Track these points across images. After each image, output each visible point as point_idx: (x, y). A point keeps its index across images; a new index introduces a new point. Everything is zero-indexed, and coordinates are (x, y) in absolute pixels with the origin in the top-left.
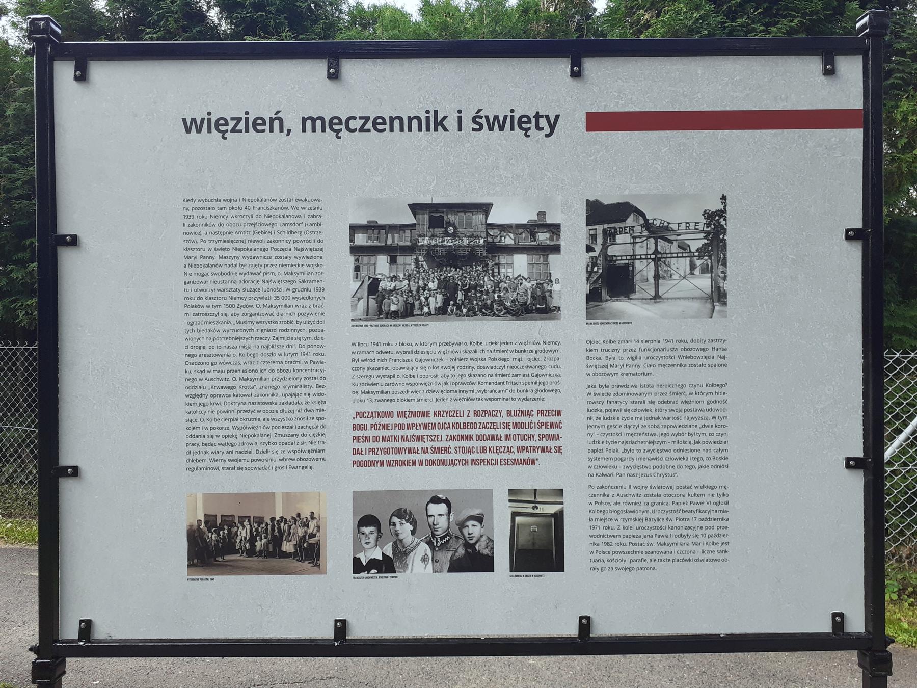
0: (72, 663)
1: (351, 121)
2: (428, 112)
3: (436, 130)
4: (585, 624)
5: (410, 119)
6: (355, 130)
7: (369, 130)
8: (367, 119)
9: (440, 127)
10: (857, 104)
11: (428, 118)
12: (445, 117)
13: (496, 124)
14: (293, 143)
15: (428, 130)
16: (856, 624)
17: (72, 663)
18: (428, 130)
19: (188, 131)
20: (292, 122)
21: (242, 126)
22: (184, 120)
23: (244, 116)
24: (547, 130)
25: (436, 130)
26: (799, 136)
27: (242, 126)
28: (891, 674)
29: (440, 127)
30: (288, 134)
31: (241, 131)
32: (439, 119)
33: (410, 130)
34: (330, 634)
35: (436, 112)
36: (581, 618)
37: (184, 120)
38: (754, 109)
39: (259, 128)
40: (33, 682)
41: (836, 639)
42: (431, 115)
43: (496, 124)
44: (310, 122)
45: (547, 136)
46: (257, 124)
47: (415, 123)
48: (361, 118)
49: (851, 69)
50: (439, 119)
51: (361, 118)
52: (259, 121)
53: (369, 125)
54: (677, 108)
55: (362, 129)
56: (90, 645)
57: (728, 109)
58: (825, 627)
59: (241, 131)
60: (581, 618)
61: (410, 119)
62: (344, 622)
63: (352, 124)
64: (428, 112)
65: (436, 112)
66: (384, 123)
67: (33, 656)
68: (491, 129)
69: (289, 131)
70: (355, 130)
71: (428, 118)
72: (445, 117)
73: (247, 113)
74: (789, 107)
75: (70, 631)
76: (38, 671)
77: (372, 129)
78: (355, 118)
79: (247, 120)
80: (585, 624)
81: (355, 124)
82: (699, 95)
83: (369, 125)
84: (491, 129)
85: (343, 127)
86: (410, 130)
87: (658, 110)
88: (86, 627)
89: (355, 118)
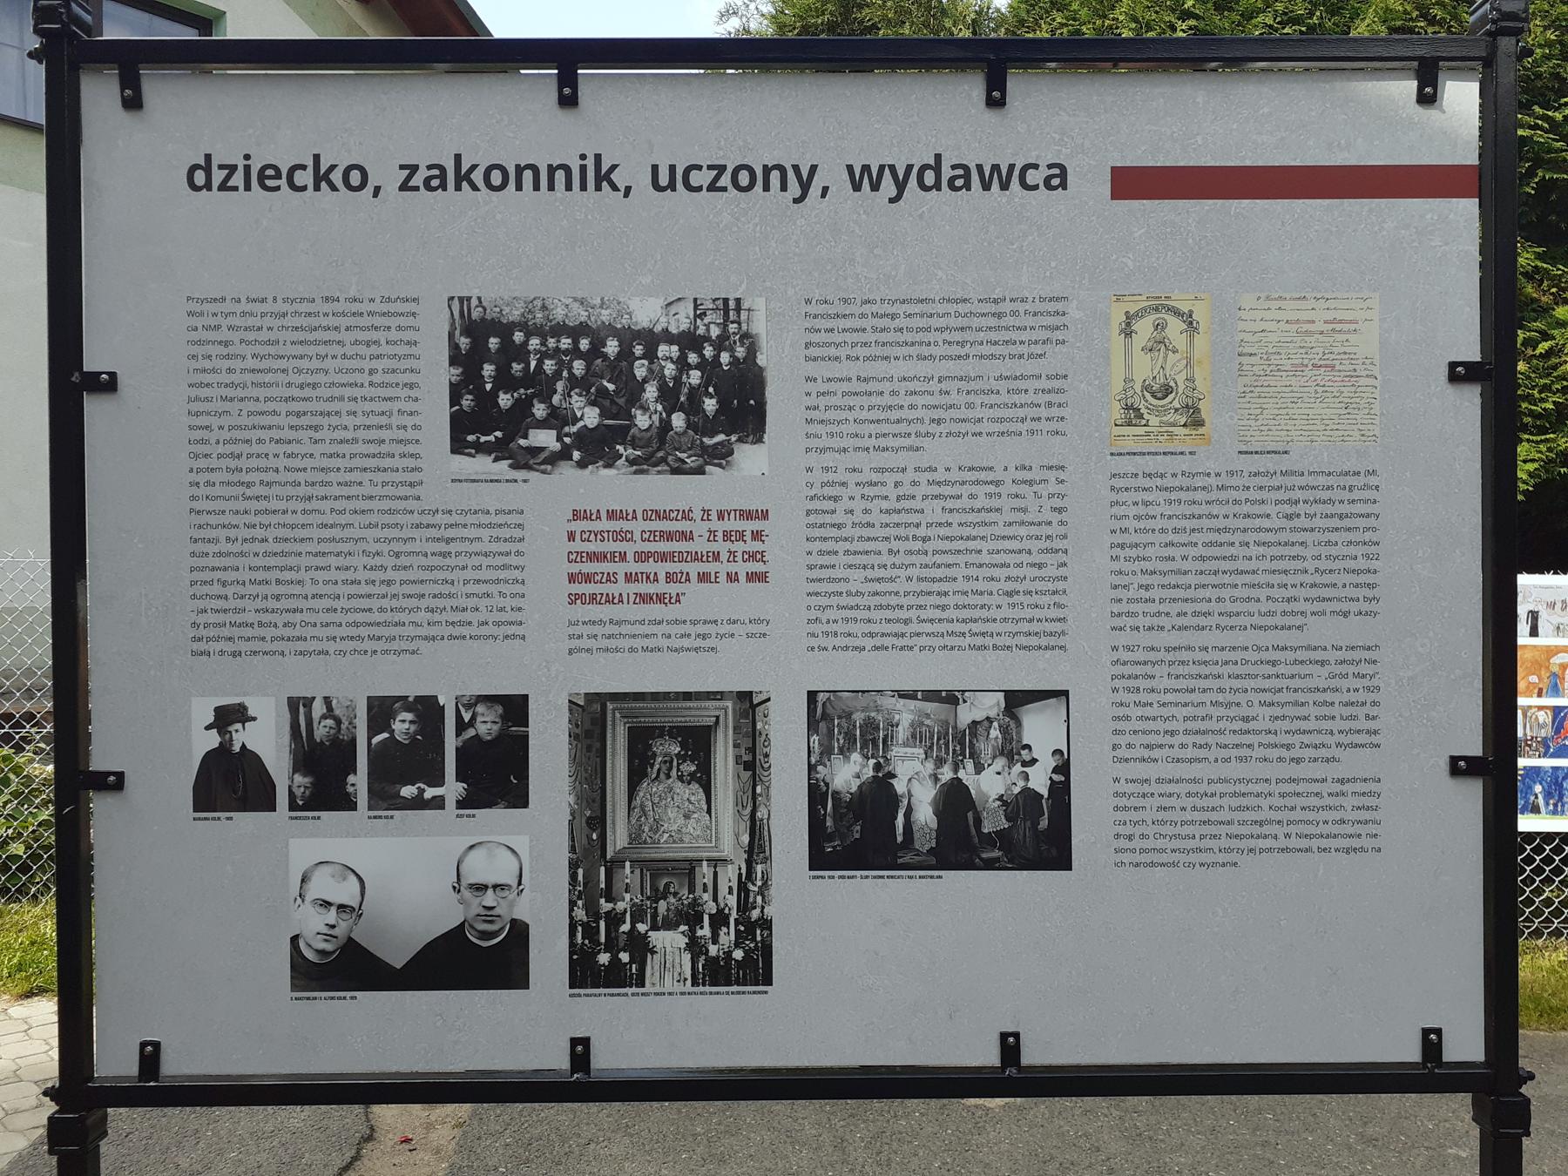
0: (120, 1118)
1: (694, 173)
2: (583, 157)
3: (598, 188)
4: (1010, 1046)
5: (552, 170)
6: (699, 189)
7: (724, 189)
8: (721, 169)
9: (465, 184)
10: (1466, 152)
11: (583, 169)
12: (614, 167)
13: (866, 180)
14: (499, 217)
15: (583, 187)
16: (1466, 1044)
17: (120, 1118)
18: (583, 187)
19: (857, 187)
20: (832, 175)
21: (238, 179)
22: (850, 168)
23: (241, 163)
24: (794, 189)
25: (598, 188)
26: (1371, 211)
27: (238, 179)
28: (1528, 1134)
29: (465, 184)
30: (626, 195)
31: (235, 189)
32: (463, 171)
33: (551, 187)
34: (992, 1058)
35: (598, 157)
36: (143, 1045)
37: (850, 168)
38: (1293, 164)
39: (269, 183)
40: (51, 1152)
41: (1429, 1073)
42: (590, 163)
43: (866, 180)
44: (862, 178)
45: (796, 201)
46: (267, 177)
47: (560, 176)
48: (710, 167)
49: (1462, 97)
50: (463, 171)
51: (710, 167)
52: (270, 172)
53: (725, 180)
54: (1161, 161)
55: (713, 187)
56: (153, 1087)
57: (1248, 163)
58: (1411, 1052)
59: (235, 189)
60: (143, 1045)
61: (552, 170)
62: (157, 1046)
63: (696, 178)
64: (583, 157)
65: (598, 157)
66: (278, 176)
67: (51, 1107)
68: (986, 186)
69: (377, 190)
70: (699, 189)
71: (583, 169)
72: (614, 167)
73: (247, 157)
74: (1352, 161)
75: (114, 1059)
76: (57, 1132)
77: (730, 187)
78: (699, 168)
79: (247, 169)
80: (1010, 1046)
81: (700, 178)
82: (1199, 139)
83: (725, 180)
84: (986, 186)
85: (283, 182)
86: (551, 187)
87: (1128, 164)
88: (150, 1057)
89: (699, 168)
